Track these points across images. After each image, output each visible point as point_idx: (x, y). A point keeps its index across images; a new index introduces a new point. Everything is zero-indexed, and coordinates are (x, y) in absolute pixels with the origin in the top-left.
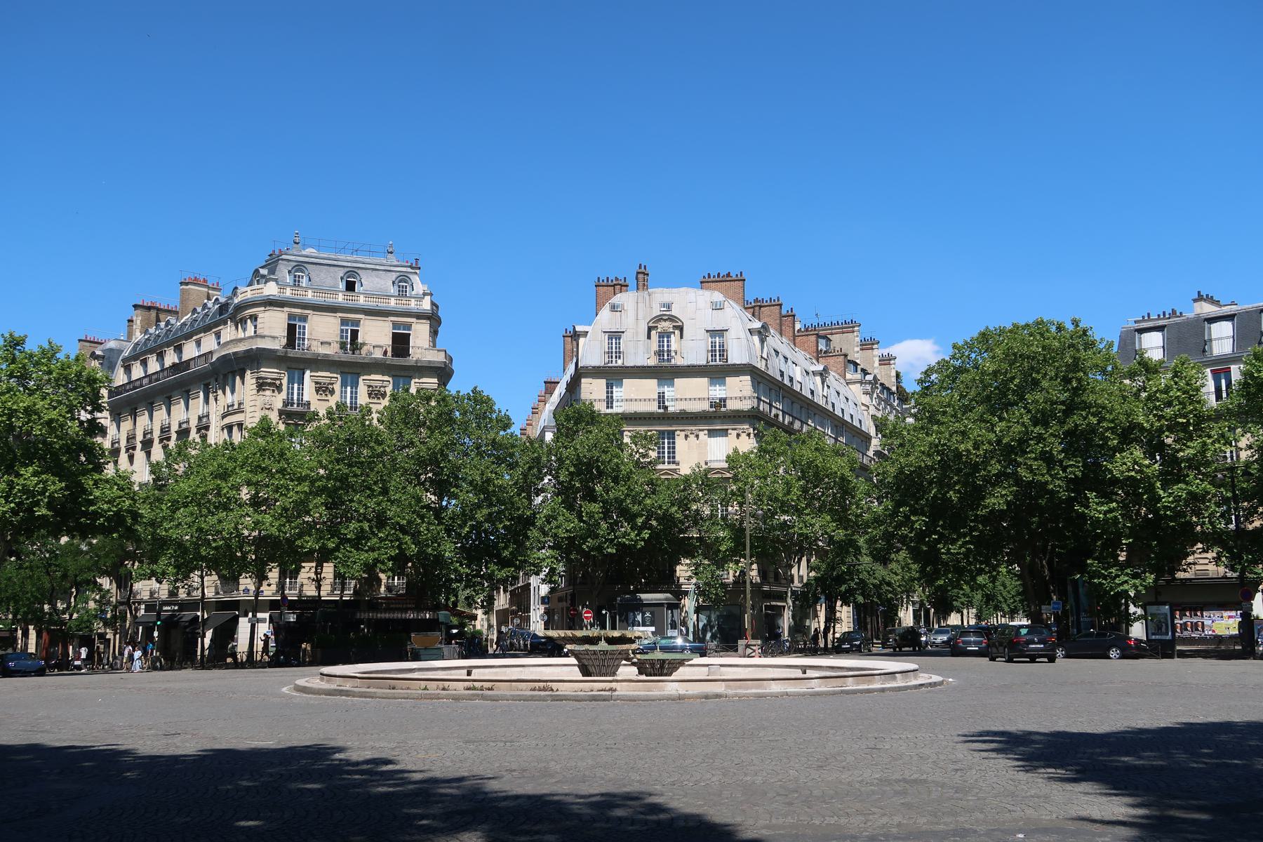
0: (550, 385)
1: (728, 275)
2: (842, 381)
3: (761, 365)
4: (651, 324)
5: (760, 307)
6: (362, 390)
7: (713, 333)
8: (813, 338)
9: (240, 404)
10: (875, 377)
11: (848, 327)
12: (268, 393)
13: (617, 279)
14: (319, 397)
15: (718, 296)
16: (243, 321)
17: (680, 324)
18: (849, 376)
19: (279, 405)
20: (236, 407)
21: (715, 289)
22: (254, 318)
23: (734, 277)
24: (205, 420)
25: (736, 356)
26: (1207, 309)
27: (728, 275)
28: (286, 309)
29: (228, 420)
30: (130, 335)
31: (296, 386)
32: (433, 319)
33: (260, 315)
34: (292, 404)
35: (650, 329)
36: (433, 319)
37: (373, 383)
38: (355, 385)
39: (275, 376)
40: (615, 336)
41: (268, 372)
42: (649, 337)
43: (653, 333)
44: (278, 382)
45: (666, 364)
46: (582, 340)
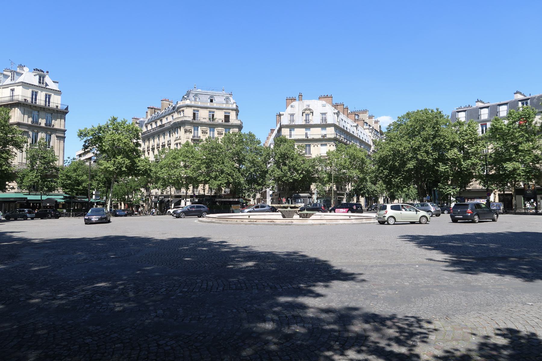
0: (272, 131)
1: (327, 96)
2: (363, 128)
3: (337, 124)
4: (303, 111)
5: (337, 105)
6: (216, 132)
7: (322, 114)
8: (354, 115)
9: (180, 137)
10: (373, 127)
11: (365, 111)
12: (188, 134)
13: (293, 97)
14: (203, 135)
15: (324, 102)
16: (180, 112)
17: (312, 111)
18: (365, 127)
19: (191, 137)
20: (179, 138)
21: (323, 100)
22: (183, 111)
23: (329, 96)
24: (169, 142)
25: (329, 121)
26: (480, 105)
27: (327, 96)
28: (192, 108)
29: (176, 142)
30: (147, 116)
31: (196, 131)
32: (237, 111)
33: (185, 110)
34: (195, 137)
35: (303, 113)
36: (237, 111)
37: (219, 130)
38: (214, 131)
39: (190, 128)
40: (292, 115)
41: (188, 127)
42: (303, 115)
43: (304, 114)
44: (191, 130)
45: (308, 124)
46: (282, 117)
